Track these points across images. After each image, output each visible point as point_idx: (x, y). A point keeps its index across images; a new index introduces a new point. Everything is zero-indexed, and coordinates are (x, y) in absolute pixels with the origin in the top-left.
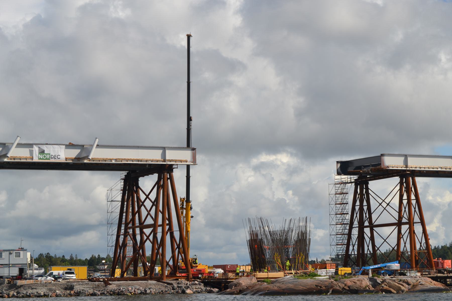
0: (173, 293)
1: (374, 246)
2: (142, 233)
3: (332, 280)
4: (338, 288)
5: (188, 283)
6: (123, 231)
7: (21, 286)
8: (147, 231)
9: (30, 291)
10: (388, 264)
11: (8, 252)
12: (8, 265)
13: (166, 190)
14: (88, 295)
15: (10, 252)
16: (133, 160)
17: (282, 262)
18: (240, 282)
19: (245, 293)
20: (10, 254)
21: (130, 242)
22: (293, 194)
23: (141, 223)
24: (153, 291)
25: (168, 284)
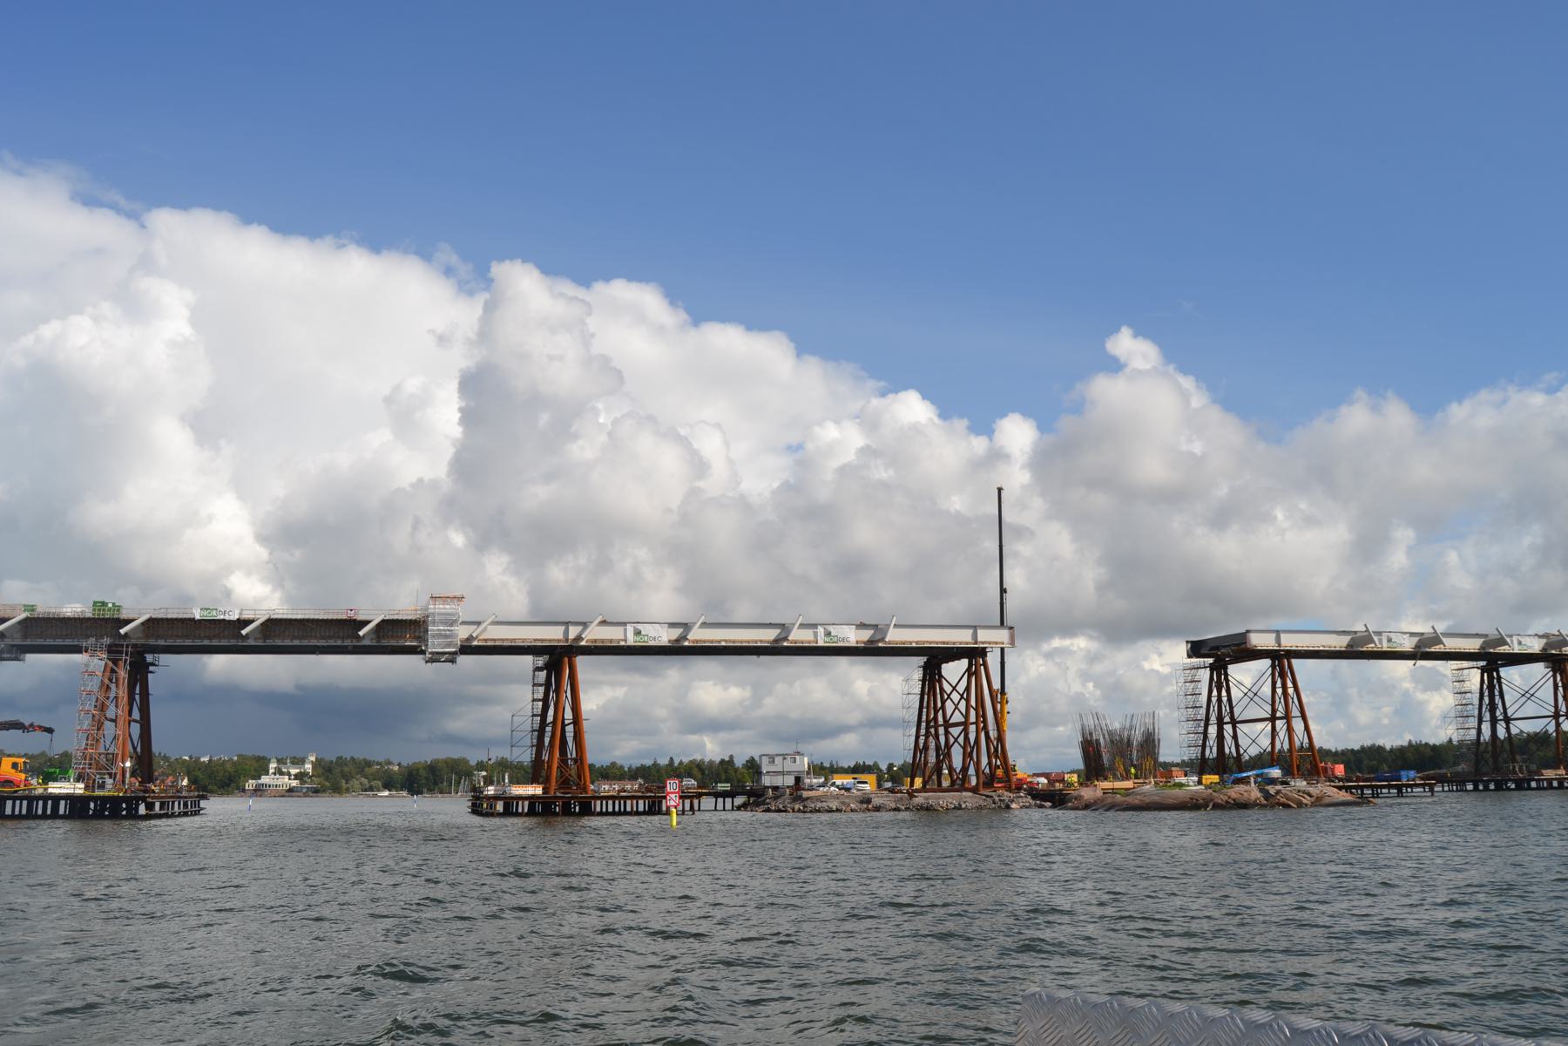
0: (994, 809)
1: (1237, 746)
2: (947, 733)
3: (1210, 791)
4: (1220, 801)
5: (1011, 795)
6: (923, 731)
7: (808, 798)
8: (955, 731)
9: (819, 805)
10: (1266, 771)
11: (781, 757)
12: (783, 773)
13: (979, 679)
14: (890, 810)
15: (784, 757)
16: (937, 643)
17: (1125, 769)
18: (1082, 794)
19: (1094, 808)
20: (784, 759)
21: (932, 744)
22: (1094, 687)
23: (946, 721)
24: (969, 805)
25: (987, 796)
